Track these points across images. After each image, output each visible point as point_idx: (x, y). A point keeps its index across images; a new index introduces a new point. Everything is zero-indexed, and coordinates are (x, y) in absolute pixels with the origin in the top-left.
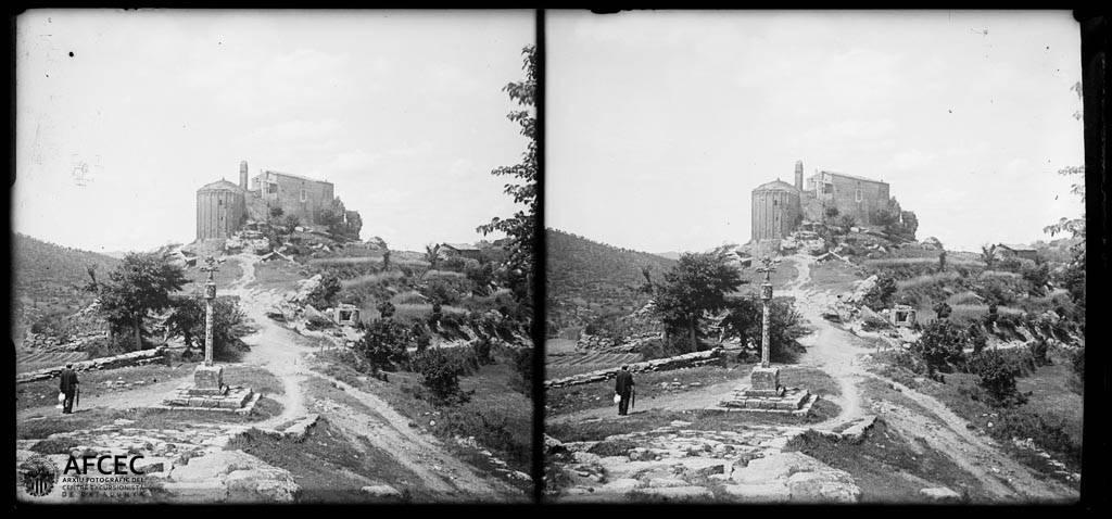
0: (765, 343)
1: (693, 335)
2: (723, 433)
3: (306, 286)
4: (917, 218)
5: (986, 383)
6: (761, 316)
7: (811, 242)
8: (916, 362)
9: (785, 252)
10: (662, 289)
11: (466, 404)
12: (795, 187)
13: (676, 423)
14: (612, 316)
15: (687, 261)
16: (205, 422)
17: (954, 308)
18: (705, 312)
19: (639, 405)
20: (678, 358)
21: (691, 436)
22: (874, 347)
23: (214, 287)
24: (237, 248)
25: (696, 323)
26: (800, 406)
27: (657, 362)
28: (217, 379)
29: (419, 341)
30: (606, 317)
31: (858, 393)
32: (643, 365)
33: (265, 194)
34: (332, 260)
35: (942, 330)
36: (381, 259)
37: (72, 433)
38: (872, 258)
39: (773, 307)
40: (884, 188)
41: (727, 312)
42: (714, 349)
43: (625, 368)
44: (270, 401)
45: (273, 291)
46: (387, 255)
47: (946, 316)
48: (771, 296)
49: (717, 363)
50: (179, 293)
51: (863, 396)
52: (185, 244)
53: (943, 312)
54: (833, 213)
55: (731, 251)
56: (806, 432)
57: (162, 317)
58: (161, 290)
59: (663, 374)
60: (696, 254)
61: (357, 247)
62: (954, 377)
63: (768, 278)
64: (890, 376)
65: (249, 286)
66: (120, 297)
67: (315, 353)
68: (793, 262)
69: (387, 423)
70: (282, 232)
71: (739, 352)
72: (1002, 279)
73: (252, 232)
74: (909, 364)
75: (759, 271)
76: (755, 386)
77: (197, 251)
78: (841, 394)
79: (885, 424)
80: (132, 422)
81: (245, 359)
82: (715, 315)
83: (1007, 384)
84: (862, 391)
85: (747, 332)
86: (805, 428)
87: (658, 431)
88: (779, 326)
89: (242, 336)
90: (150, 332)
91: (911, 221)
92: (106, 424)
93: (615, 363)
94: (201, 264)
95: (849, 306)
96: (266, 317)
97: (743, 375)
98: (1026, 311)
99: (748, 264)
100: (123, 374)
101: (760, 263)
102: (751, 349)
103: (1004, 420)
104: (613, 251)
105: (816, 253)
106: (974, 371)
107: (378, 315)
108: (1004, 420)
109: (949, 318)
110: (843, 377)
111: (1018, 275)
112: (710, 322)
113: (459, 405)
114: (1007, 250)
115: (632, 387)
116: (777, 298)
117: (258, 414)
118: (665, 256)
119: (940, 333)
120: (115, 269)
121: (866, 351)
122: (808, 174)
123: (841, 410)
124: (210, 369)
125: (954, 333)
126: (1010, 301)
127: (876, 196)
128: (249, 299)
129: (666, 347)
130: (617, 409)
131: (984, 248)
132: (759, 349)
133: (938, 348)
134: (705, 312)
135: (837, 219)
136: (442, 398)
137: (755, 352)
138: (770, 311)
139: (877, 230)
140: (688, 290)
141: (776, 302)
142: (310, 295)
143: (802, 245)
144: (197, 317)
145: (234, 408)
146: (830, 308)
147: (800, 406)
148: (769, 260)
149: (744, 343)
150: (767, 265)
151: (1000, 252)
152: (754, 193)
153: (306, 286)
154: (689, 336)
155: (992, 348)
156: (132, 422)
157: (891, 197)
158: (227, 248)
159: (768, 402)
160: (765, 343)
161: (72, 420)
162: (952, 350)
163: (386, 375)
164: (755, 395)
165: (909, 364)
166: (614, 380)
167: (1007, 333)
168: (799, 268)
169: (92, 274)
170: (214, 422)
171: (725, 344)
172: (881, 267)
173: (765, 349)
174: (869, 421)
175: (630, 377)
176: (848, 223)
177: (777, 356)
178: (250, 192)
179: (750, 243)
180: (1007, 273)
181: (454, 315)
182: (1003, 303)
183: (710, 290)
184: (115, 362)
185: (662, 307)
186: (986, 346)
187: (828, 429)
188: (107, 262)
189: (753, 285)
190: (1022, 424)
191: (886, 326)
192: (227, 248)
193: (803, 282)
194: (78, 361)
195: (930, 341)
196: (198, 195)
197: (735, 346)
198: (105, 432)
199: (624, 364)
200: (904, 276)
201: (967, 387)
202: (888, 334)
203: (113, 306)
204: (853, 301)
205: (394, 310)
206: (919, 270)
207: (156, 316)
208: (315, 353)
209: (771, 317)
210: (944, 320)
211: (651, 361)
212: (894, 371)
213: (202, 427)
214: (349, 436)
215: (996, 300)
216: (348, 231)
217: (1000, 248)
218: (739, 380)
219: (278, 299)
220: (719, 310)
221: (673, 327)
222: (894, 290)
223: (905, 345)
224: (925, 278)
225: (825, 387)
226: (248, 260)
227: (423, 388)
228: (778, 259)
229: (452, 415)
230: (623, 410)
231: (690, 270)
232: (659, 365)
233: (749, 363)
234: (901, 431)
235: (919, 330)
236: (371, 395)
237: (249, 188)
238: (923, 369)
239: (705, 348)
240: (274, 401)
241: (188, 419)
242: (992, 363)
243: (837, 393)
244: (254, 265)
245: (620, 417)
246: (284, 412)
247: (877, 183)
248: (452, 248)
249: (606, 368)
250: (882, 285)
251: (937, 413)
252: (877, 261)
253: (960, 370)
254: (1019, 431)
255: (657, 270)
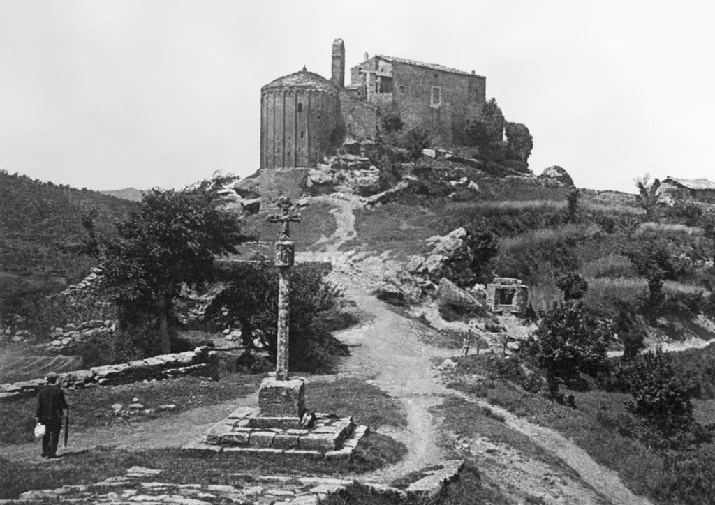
0: (281, 339)
1: (164, 324)
2: (212, 487)
3: (440, 247)
4: (531, 133)
5: (643, 409)
6: (275, 293)
7: (357, 173)
8: (528, 372)
9: (316, 189)
10: (114, 250)
11: (704, 445)
12: (331, 81)
13: (135, 471)
14: (36, 294)
15: (156, 203)
16: (275, 472)
17: (592, 283)
18: (184, 287)
19: (74, 442)
20: (139, 363)
21: (160, 492)
22: (459, 347)
23: (292, 247)
24: (327, 184)
25: (169, 306)
26: (339, 443)
27: (105, 370)
28: (296, 402)
29: (627, 341)
30: (23, 295)
31: (434, 423)
32: (82, 374)
33: (371, 95)
34: (484, 204)
35: (572, 318)
36: (563, 204)
37: (58, 491)
38: (456, 199)
39: (294, 280)
40: (477, 82)
41: (219, 288)
42: (198, 349)
43: (52, 380)
44: (382, 438)
45: (385, 254)
46: (574, 196)
47: (578, 296)
48: (292, 261)
49: (204, 373)
50: (233, 258)
51: (441, 428)
52: (243, 177)
53: (574, 290)
54: (394, 124)
55: (227, 188)
56: (348, 486)
57: (203, 298)
58: (203, 252)
59: (116, 389)
60: (170, 192)
61: (524, 183)
62: (592, 397)
63: (287, 233)
64: (485, 395)
65: (347, 246)
66: (134, 265)
67: (454, 359)
68: (326, 206)
69: (575, 475)
70: (402, 158)
71: (239, 353)
72: (671, 237)
73: (351, 157)
74: (518, 377)
75: (273, 220)
76: (265, 409)
77: (260, 189)
78: (405, 424)
79: (477, 474)
80: (156, 472)
81: (341, 367)
82: (201, 293)
83: (679, 409)
84: (441, 420)
85: (252, 321)
86: (348, 480)
87: (106, 483)
88: (306, 310)
89: (335, 329)
90: (185, 322)
91: (522, 140)
92: (114, 475)
93: (36, 371)
94: (268, 209)
95: (419, 279)
96: (374, 298)
97: (245, 393)
98: (709, 289)
99: (253, 209)
100: (140, 393)
101: (273, 207)
102: (258, 350)
103: (672, 468)
104: (35, 186)
105: (365, 191)
106: (623, 388)
107: (559, 295)
108: (672, 468)
109: (583, 300)
110: (410, 396)
111: (697, 230)
112: (192, 304)
113: (693, 446)
114: (678, 189)
115: (65, 411)
116: (300, 265)
117: (362, 460)
118: (118, 197)
119: (568, 324)
120: (127, 217)
121: (446, 353)
122: (352, 60)
123: (405, 451)
124: (284, 384)
125: (592, 324)
126: (683, 272)
127: (465, 98)
128: (346, 267)
129: (120, 347)
130: (39, 447)
131: (640, 185)
132: (272, 349)
133: (564, 349)
134: (184, 287)
135: (400, 136)
136: (666, 436)
137: (265, 354)
138: (290, 286)
139: (466, 154)
140: (157, 250)
141: (300, 272)
142: (446, 263)
143: (342, 178)
144: (262, 297)
145: (324, 450)
146: (387, 280)
147: (339, 443)
148: (288, 202)
149: (247, 339)
150: (286, 210)
151: (668, 191)
152: (266, 91)
153: (440, 247)
154: (157, 327)
155: (654, 350)
156: (156, 472)
157: (488, 98)
158: (310, 184)
159: (286, 436)
160: (281, 339)
161: (57, 468)
162: (587, 352)
163: (572, 398)
164: (266, 426)
165: (518, 377)
166: (35, 400)
167: (679, 325)
168: (337, 215)
169: (88, 225)
170: (290, 473)
171: (216, 341)
172: (472, 214)
173: (281, 350)
174: (451, 470)
175: (62, 394)
176: (418, 142)
177: (300, 362)
178: (347, 91)
179: (257, 174)
180: (678, 227)
181: (682, 296)
182: (672, 276)
183: (191, 251)
184: (126, 371)
185: (113, 279)
186: (643, 347)
187: (385, 482)
188: (112, 207)
189: (263, 244)
190: (701, 476)
191: (479, 312)
192: (310, 184)
193: (345, 238)
194: (66, 370)
195: (551, 335)
196: (263, 95)
197: (231, 345)
198: (112, 489)
199: (52, 374)
200: (509, 230)
201: (612, 415)
202: (482, 325)
203: (123, 280)
204: (426, 270)
205: (585, 287)
206: (532, 221)
207: (193, 296)
208: (454, 359)
209: (291, 297)
210: (575, 302)
211: (95, 369)
212: (492, 387)
213: (272, 482)
214: (514, 497)
215: (661, 271)
216: (508, 157)
217: (668, 186)
218: (239, 400)
219: (393, 268)
220: (206, 284)
221: (130, 314)
222: (493, 252)
223: (509, 344)
224: (543, 234)
225: (380, 413)
226: (346, 204)
227: (635, 420)
228: (303, 201)
229: (682, 464)
230: (49, 445)
231: (160, 218)
232: (109, 375)
233: (255, 371)
234: (502, 487)
235: (534, 319)
236: (549, 431)
237: (348, 82)
238: (540, 384)
239: (186, 346)
240: (390, 439)
241: (248, 468)
242: (653, 376)
243: (400, 422)
244: (354, 212)
245: (45, 460)
246: (410, 456)
247: (464, 75)
248: (680, 186)
249: (21, 379)
250: (472, 244)
251: (563, 457)
252: (465, 205)
253: (601, 387)
254: (697, 486)
255: (105, 219)
